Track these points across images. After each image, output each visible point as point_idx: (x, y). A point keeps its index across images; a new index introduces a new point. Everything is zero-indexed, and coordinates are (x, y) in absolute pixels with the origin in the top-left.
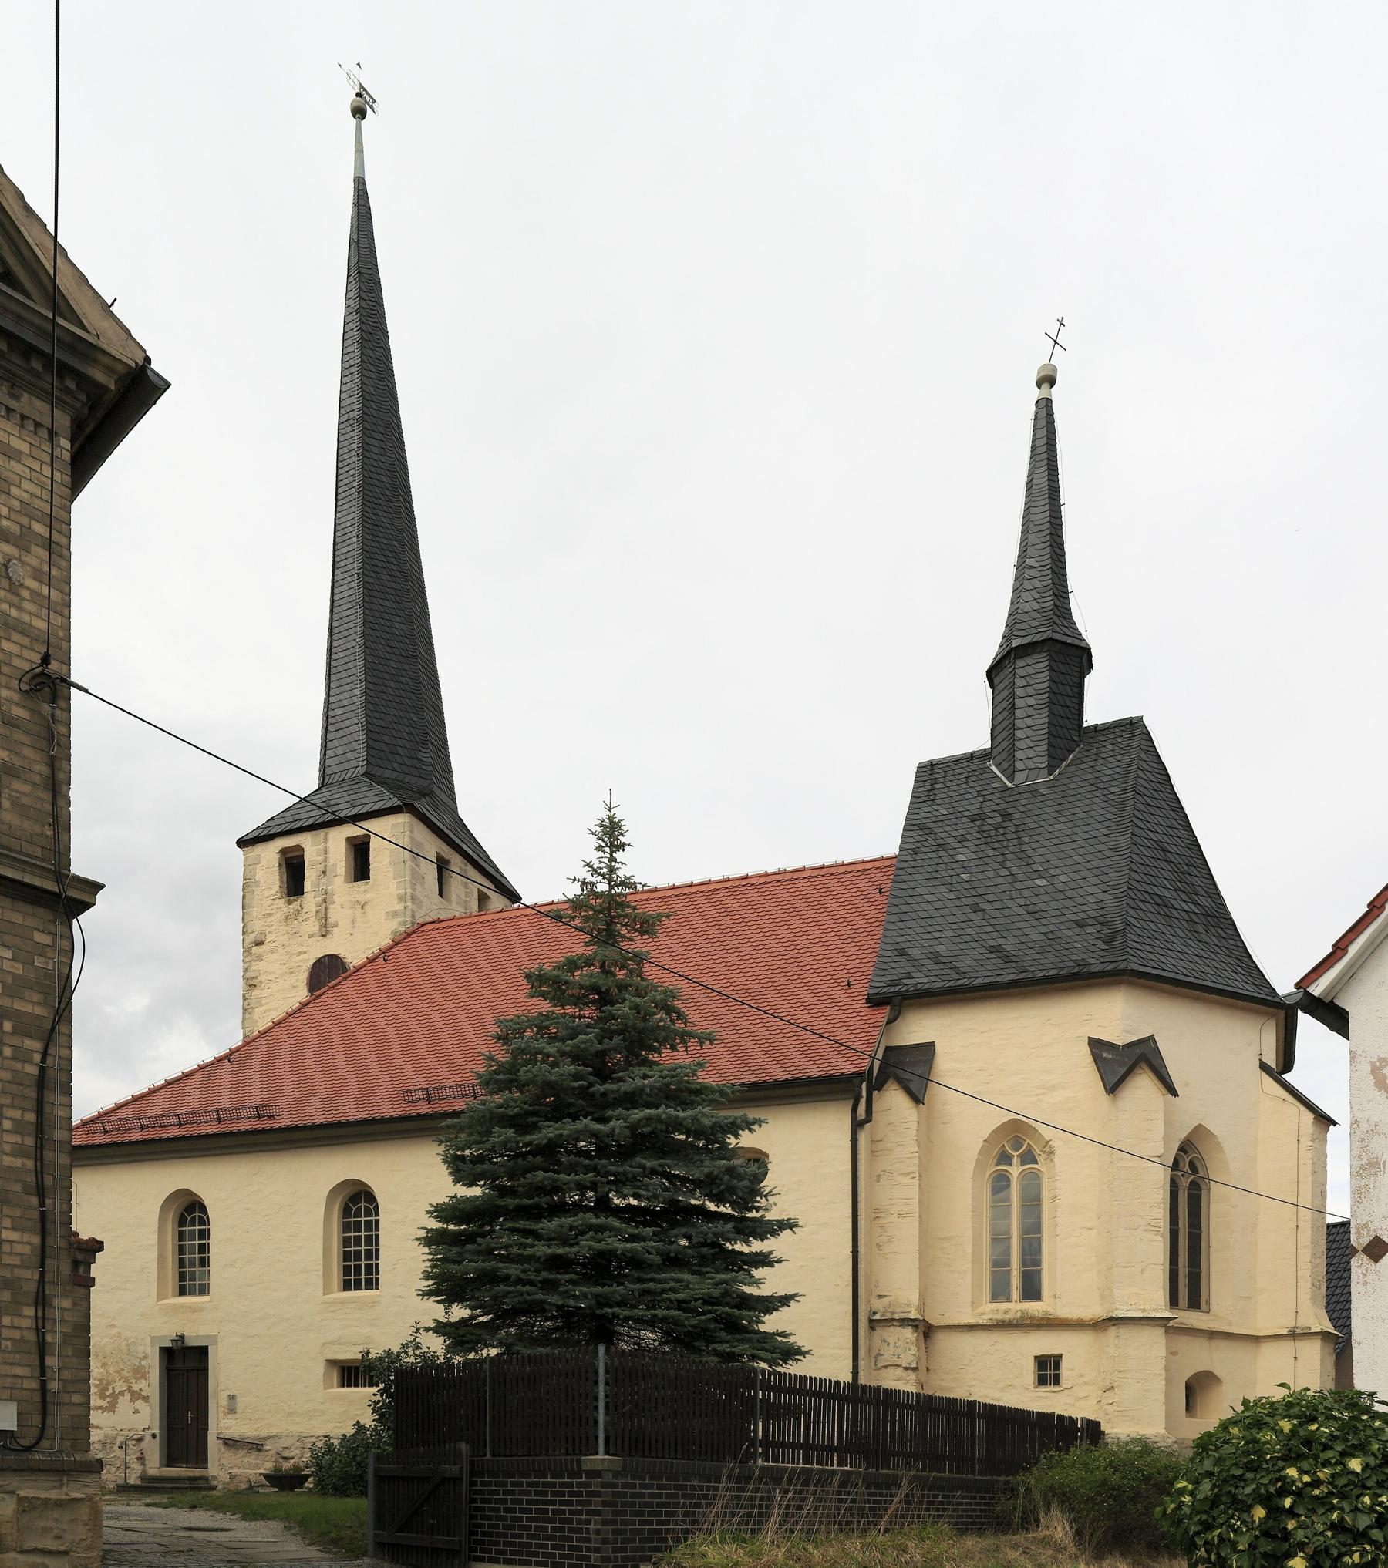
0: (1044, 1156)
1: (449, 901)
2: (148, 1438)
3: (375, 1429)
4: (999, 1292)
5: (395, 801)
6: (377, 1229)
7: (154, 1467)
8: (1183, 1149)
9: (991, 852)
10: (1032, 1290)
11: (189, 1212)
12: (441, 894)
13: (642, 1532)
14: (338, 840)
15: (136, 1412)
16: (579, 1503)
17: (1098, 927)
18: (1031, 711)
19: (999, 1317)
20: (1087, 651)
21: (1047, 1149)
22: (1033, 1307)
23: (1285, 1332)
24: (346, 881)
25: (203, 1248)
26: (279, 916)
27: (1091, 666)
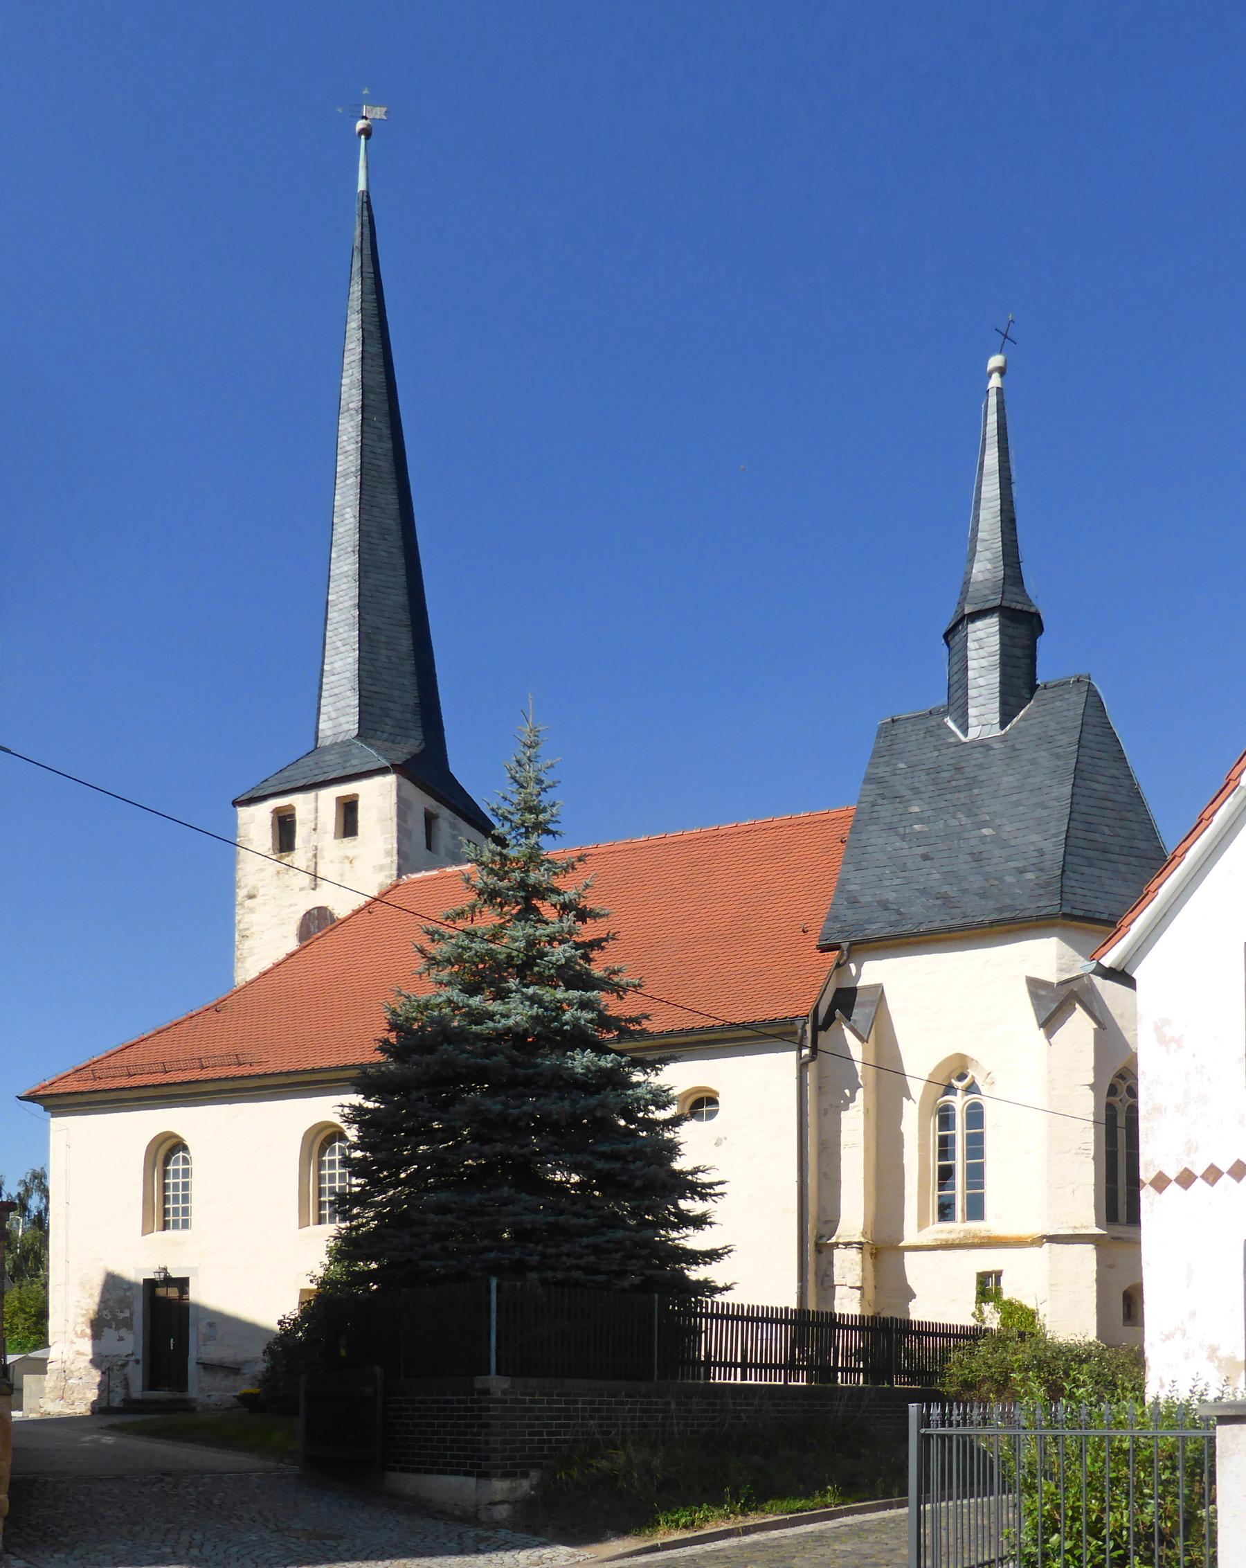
2: (131, 1364)
3: (999, 1330)
4: (946, 1211)
5: (384, 763)
10: (976, 1210)
11: (168, 1152)
12: (429, 847)
13: (532, 1441)
14: (329, 797)
15: (121, 1339)
17: (1039, 873)
18: (983, 672)
19: (944, 1236)
20: (1037, 615)
22: (975, 1226)
24: (336, 838)
25: (186, 1186)
27: (1042, 629)
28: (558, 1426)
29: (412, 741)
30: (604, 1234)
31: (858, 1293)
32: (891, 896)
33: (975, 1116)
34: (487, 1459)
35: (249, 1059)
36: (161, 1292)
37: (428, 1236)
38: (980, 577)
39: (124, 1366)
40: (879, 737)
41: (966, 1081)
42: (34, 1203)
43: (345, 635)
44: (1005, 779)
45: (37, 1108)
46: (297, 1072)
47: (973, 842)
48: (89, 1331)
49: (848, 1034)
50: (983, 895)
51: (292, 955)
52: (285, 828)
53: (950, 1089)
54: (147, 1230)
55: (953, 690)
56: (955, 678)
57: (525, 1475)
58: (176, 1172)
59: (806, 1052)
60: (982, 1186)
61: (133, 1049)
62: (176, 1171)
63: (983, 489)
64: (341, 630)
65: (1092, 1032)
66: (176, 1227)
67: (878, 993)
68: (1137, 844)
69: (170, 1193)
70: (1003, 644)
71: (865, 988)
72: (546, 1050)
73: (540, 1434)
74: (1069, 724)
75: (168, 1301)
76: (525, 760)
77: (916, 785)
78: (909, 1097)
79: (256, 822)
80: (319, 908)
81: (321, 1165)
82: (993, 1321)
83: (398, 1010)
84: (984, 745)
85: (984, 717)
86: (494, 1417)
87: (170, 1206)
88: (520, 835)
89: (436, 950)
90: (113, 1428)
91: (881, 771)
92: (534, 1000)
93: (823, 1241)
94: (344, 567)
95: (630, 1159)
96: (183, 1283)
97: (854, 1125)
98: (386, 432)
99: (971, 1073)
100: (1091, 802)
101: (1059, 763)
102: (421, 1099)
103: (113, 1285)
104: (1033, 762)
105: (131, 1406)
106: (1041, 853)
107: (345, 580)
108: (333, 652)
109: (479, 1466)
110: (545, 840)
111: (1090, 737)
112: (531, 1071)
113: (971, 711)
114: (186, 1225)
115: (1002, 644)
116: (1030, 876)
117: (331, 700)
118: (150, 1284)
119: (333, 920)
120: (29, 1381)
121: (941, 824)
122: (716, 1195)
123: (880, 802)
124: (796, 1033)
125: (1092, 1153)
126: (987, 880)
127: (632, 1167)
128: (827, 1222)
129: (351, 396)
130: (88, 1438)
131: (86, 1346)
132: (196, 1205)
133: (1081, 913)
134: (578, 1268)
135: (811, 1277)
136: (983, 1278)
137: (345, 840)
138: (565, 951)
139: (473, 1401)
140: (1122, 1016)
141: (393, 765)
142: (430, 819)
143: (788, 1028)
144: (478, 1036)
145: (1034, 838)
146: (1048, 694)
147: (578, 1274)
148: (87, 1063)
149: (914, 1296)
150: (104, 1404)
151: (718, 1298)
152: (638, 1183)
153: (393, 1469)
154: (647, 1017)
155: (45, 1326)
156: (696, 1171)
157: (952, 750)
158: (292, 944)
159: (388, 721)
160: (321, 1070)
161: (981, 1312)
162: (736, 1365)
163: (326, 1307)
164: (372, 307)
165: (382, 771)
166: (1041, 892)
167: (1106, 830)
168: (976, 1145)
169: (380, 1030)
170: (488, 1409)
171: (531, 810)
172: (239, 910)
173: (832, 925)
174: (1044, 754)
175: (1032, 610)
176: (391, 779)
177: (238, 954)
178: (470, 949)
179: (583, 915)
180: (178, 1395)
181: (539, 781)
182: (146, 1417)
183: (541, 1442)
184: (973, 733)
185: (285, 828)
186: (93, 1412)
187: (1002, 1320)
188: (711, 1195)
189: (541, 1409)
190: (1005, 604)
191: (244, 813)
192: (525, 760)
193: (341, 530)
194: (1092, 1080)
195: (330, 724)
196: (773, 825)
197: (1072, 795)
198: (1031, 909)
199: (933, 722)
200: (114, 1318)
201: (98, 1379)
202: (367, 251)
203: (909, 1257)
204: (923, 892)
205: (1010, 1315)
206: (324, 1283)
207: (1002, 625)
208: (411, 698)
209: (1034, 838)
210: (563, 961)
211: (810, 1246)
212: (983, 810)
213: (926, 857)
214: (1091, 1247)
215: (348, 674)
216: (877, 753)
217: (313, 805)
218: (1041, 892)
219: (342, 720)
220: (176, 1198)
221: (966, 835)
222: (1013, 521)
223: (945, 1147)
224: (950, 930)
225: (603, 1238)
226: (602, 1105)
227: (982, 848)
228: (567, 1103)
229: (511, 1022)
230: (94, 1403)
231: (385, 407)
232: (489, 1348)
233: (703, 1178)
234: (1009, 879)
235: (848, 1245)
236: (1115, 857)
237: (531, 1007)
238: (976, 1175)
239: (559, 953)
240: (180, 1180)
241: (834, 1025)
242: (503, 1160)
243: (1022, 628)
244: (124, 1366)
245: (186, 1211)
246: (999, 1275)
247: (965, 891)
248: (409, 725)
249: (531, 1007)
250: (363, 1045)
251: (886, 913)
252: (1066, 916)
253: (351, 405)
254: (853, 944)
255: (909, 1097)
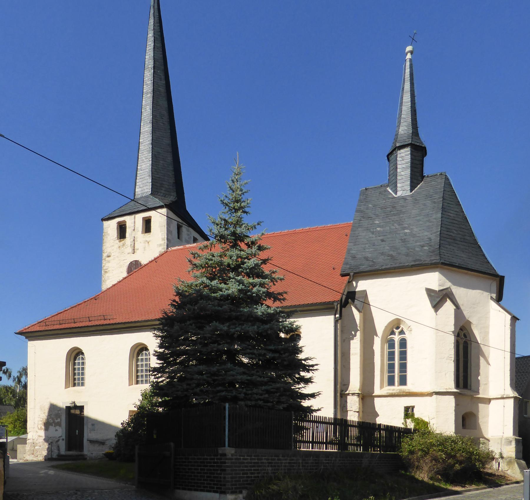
0: (408, 332)
1: (181, 240)
2: (61, 441)
4: (391, 382)
5: (162, 204)
6: (149, 361)
7: (63, 451)
8: (461, 329)
9: (388, 220)
10: (403, 381)
11: (76, 354)
12: (179, 238)
13: (244, 477)
14: (139, 218)
15: (56, 430)
16: (217, 466)
19: (391, 392)
20: (425, 148)
21: (409, 329)
22: (403, 388)
23: (500, 397)
24: (142, 233)
25: (83, 369)
26: (117, 246)
28: (254, 470)
29: (172, 197)
30: (271, 385)
31: (357, 414)
32: (369, 255)
33: (403, 343)
34: (225, 485)
35: (109, 317)
36: (73, 411)
37: (194, 385)
38: (402, 132)
39: (58, 441)
40: (360, 195)
41: (400, 330)
42: (23, 379)
43: (146, 155)
44: (413, 211)
45: (23, 337)
46: (128, 323)
47: (401, 235)
48: (43, 427)
49: (354, 309)
50: (407, 255)
51: (125, 278)
52: (122, 231)
53: (393, 333)
54: (67, 386)
55: (391, 176)
56: (392, 172)
57: (241, 492)
58: (79, 363)
59: (337, 316)
60: (406, 372)
61: (62, 314)
62: (79, 363)
63: (404, 98)
64: (145, 153)
65: (453, 311)
66: (79, 385)
67: (364, 293)
68: (466, 237)
69: (76, 372)
70: (412, 159)
71: (359, 291)
72: (244, 305)
73: (247, 474)
74: (438, 190)
75: (76, 415)
76: (235, 180)
77: (377, 213)
78: (377, 336)
79: (111, 227)
80: (136, 261)
81: (137, 360)
82: (411, 425)
83: (179, 287)
84: (404, 198)
85: (403, 188)
86: (228, 467)
87: (76, 377)
88: (233, 213)
89: (197, 262)
90: (53, 467)
91: (362, 208)
92: (240, 282)
93: (343, 392)
94: (146, 129)
95: (282, 352)
96: (81, 408)
97: (356, 345)
98: (163, 77)
99: (402, 326)
100: (448, 220)
101: (436, 205)
102: (191, 325)
103: (53, 408)
104: (424, 205)
105: (61, 457)
106: (430, 239)
107: (146, 134)
108: (141, 162)
109: (221, 488)
110: (244, 215)
111: (447, 196)
112: (239, 313)
113: (399, 185)
114: (83, 384)
115: (412, 159)
116: (426, 248)
117: (141, 180)
118: (68, 408)
119: (141, 265)
120: (19, 447)
121: (388, 228)
122: (314, 370)
123: (362, 219)
124: (334, 308)
125: (453, 359)
126: (408, 249)
127: (284, 356)
128: (344, 385)
129: (149, 62)
130: (43, 472)
131: (42, 433)
132: (87, 376)
133: (448, 263)
134: (260, 400)
135: (338, 407)
136: (407, 409)
137: (146, 234)
138: (254, 261)
139: (217, 459)
140: (463, 305)
141: (165, 205)
142: (179, 227)
143: (331, 306)
144: (215, 298)
145: (426, 233)
146: (429, 179)
147: (261, 403)
148: (43, 319)
149: (378, 415)
150: (50, 457)
151: (314, 414)
152: (285, 363)
153: (179, 489)
154: (286, 293)
155: (26, 425)
156: (305, 360)
157: (391, 200)
158: (125, 274)
159: (163, 189)
160: (138, 322)
161: (406, 422)
162: (309, 442)
163: (141, 417)
164: (158, 28)
165: (161, 207)
166: (431, 254)
167: (455, 231)
168: (403, 355)
169: (172, 296)
170: (225, 463)
171: (237, 201)
172: (104, 262)
173: (345, 266)
174: (428, 201)
175: (423, 146)
176: (164, 211)
177: (103, 279)
178: (212, 260)
179: (260, 248)
180: (79, 453)
181: (241, 190)
182: (67, 462)
183: (248, 477)
184: (399, 194)
185: (122, 231)
186: (45, 460)
187: (415, 426)
188: (312, 370)
189: (247, 463)
190: (413, 143)
191: (106, 224)
192: (235, 180)
193: (145, 114)
194: (453, 330)
195: (140, 189)
196: (317, 229)
197: (442, 217)
198: (428, 261)
199: (382, 189)
200: (54, 422)
201: (47, 447)
202: (156, 7)
203: (376, 400)
204: (382, 254)
205: (418, 424)
206: (140, 408)
207: (411, 151)
208: (172, 180)
209: (426, 233)
210: (253, 265)
211: (338, 394)
212: (405, 223)
213: (383, 241)
214: (453, 397)
215: (147, 170)
216: (360, 201)
217: (133, 221)
218: (431, 254)
219: (145, 188)
220: (79, 374)
221: (399, 232)
222: (415, 111)
223: (391, 356)
224: (395, 268)
225: (271, 387)
226: (271, 329)
227: (405, 237)
228: (256, 327)
229: (230, 292)
230: (45, 456)
231: (163, 67)
232: (225, 434)
233: (310, 362)
234: (417, 249)
235: (353, 394)
236: (458, 242)
237: (239, 285)
238: (403, 367)
239: (251, 263)
240: (81, 367)
241: (348, 305)
242: (225, 351)
243: (419, 152)
244: (58, 441)
245: (83, 379)
246: (413, 407)
247: (399, 254)
248: (171, 190)
249: (239, 285)
250: (162, 304)
251: (368, 262)
252: (442, 263)
253: (149, 66)
254: (355, 273)
255: (377, 336)
